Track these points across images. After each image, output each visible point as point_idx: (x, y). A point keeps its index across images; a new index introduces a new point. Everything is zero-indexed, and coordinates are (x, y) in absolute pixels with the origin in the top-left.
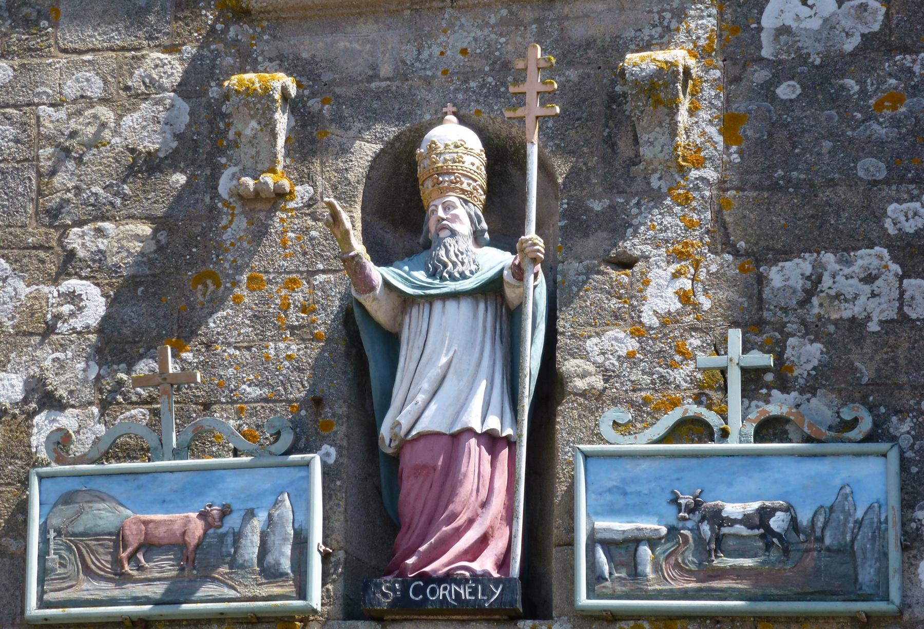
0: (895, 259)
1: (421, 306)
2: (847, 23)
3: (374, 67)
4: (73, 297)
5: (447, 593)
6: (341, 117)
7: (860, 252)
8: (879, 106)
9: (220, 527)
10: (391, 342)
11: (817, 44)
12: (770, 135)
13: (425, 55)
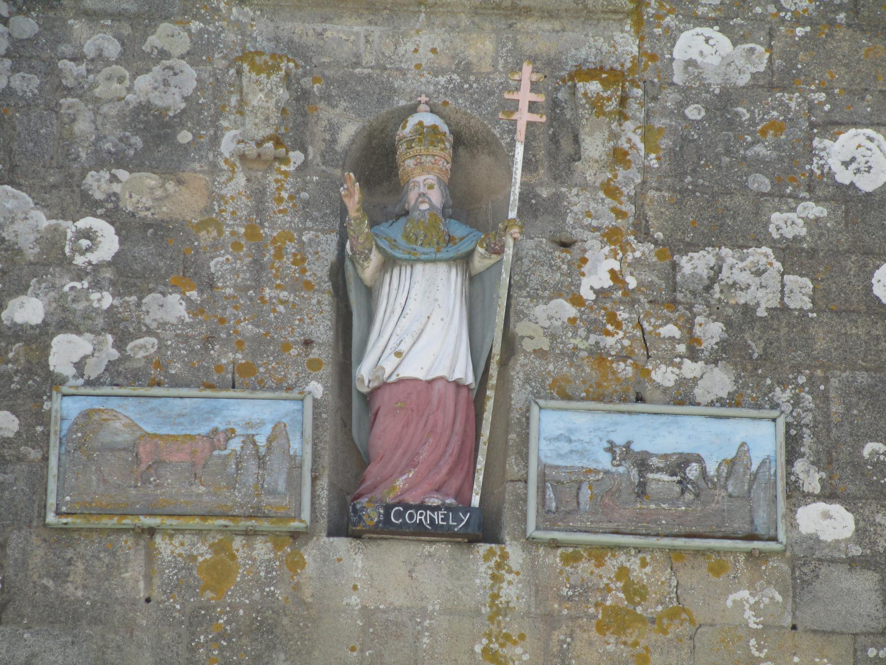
0: (777, 258)
1: (403, 268)
2: (741, 62)
3: (357, 56)
4: (88, 234)
5: (423, 518)
6: (329, 96)
7: (750, 250)
8: (764, 132)
9: (202, 596)
10: (370, 294)
11: (716, 77)
12: (681, 147)
13: (401, 50)
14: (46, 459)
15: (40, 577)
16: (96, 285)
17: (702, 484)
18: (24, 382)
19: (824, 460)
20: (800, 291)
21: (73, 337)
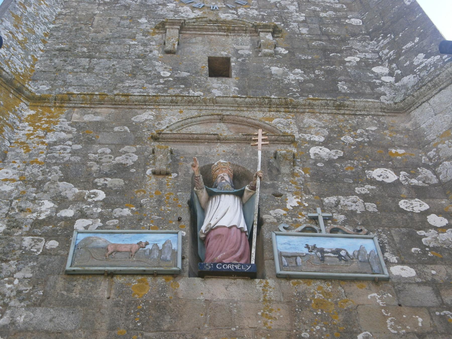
9: (145, 247)
13: (212, 151)
14: (68, 254)
15: (61, 291)
16: (96, 206)
17: (348, 258)
18: (62, 232)
19: (397, 252)
20: (372, 207)
21: (85, 220)
